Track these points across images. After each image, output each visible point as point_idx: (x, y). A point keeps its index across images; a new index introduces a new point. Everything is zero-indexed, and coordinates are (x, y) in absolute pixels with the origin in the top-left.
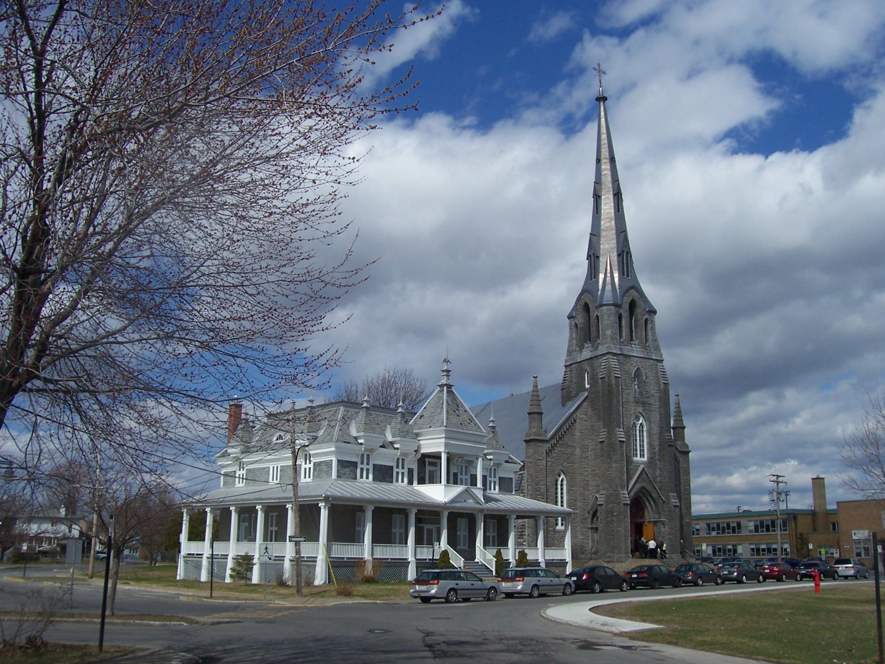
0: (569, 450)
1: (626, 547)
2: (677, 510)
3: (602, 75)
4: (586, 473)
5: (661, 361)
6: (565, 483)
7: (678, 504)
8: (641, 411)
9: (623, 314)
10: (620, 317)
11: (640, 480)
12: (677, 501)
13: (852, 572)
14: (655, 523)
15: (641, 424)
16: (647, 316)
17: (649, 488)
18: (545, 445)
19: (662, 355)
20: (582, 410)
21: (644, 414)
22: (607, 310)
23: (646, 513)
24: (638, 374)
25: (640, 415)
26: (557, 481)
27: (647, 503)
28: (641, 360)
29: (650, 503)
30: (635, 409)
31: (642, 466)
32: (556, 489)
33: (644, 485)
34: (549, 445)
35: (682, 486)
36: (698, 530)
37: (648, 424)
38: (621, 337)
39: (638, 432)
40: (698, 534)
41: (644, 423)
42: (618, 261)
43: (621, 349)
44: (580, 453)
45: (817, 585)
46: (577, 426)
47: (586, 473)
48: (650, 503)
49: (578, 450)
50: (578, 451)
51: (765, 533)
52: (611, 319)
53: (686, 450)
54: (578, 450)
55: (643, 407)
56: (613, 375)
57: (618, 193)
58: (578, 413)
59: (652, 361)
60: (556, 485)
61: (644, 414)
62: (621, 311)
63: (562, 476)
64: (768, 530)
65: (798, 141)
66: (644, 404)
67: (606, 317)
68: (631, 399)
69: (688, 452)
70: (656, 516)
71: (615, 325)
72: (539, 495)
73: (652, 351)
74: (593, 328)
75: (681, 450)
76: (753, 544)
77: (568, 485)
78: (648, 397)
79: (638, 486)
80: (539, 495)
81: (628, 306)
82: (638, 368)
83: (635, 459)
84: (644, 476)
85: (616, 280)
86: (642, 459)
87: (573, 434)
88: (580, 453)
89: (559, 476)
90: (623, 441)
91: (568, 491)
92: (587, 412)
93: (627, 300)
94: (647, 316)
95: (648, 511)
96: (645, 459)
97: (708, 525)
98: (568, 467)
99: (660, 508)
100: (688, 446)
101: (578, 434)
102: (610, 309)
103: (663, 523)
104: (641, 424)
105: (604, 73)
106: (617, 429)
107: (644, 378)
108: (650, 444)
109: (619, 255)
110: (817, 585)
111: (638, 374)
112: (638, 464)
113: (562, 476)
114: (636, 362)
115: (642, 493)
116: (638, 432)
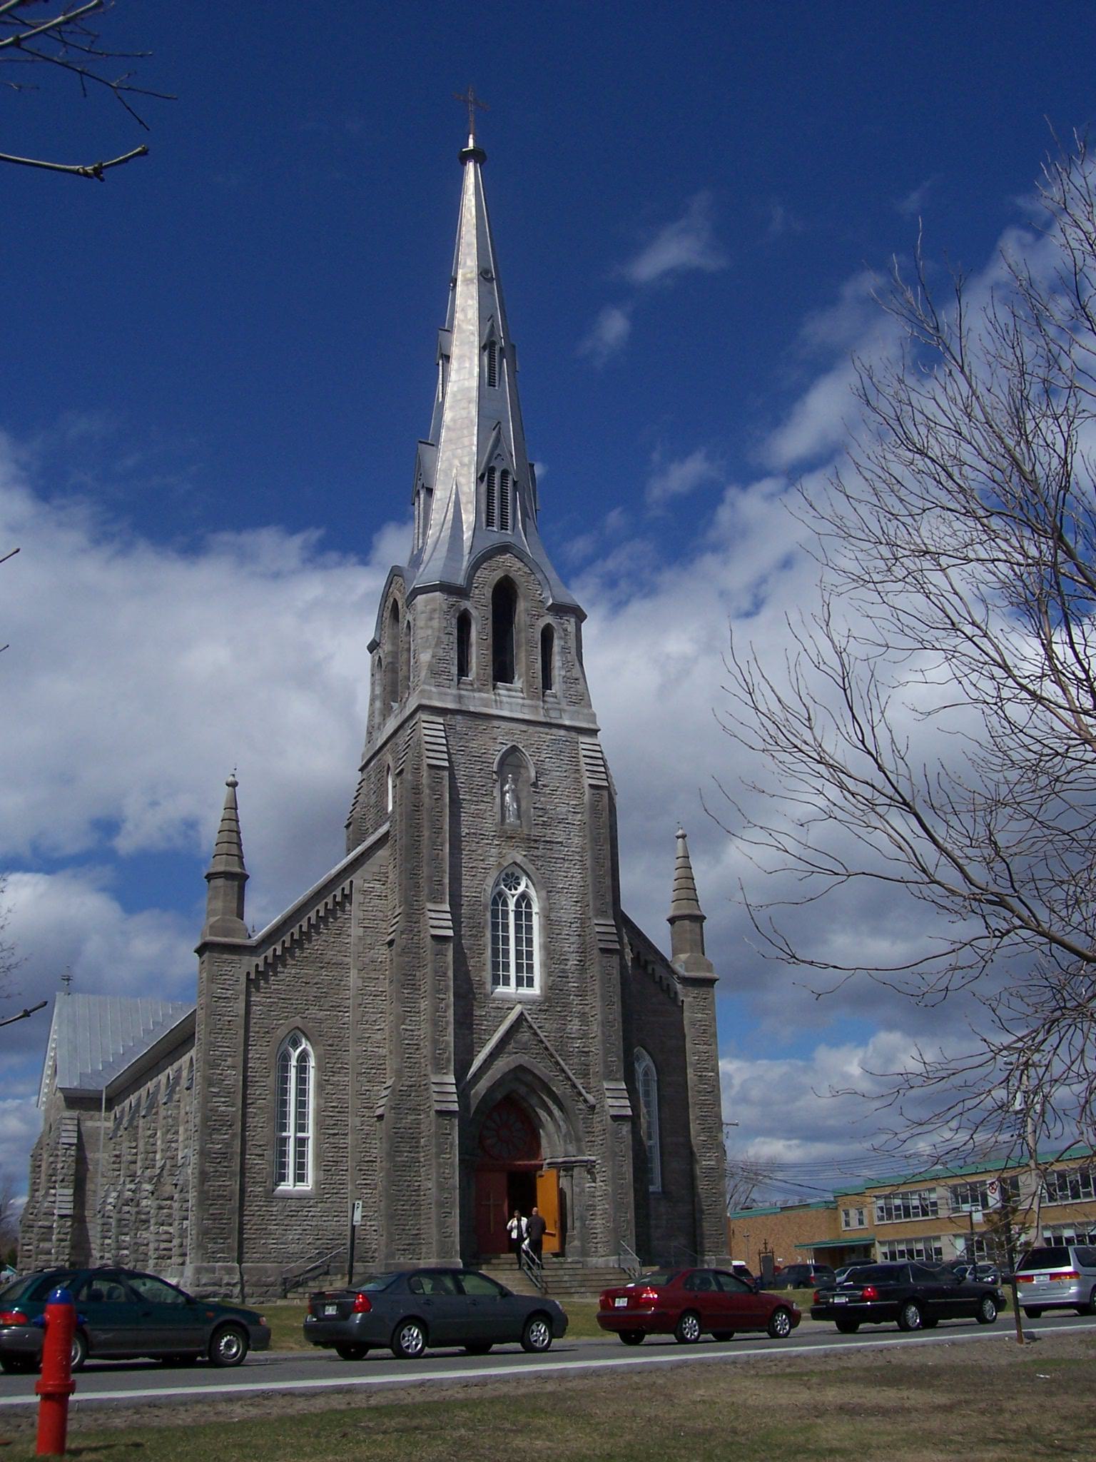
1: (445, 1236)
2: (626, 1129)
4: (378, 1036)
5: (593, 732)
6: (312, 1062)
7: (629, 1112)
8: (519, 859)
9: (474, 612)
10: (464, 622)
11: (511, 1047)
12: (627, 1103)
13: (1074, 1289)
14: (568, 1167)
16: (549, 619)
17: (542, 1068)
18: (246, 959)
19: (594, 715)
20: (370, 867)
21: (530, 868)
22: (427, 603)
23: (544, 1142)
24: (511, 761)
25: (518, 872)
26: (286, 1058)
27: (543, 1114)
28: (524, 727)
29: (550, 1113)
30: (501, 855)
31: (519, 1008)
32: (285, 1080)
33: (524, 1059)
34: (260, 960)
35: (690, 1071)
36: (934, 1204)
37: (544, 893)
38: (463, 670)
40: (935, 1212)
41: (532, 893)
43: (460, 697)
45: (57, 1398)
46: (354, 909)
47: (378, 1036)
48: (550, 1113)
49: (353, 973)
50: (353, 979)
51: (1070, 1201)
52: (435, 623)
54: (353, 973)
58: (357, 879)
59: (562, 732)
60: (285, 1068)
61: (530, 868)
62: (466, 604)
63: (305, 1044)
64: (1076, 1195)
66: (531, 842)
67: (421, 623)
68: (489, 826)
70: (572, 1149)
71: (445, 638)
72: (216, 1095)
73: (564, 706)
75: (687, 974)
76: (1046, 1228)
77: (319, 1068)
79: (503, 1064)
80: (216, 1095)
81: (488, 592)
82: (514, 749)
83: (501, 989)
84: (525, 1036)
85: (467, 535)
86: (525, 991)
89: (295, 1044)
91: (320, 1087)
92: (386, 875)
93: (489, 577)
94: (549, 619)
95: (548, 1135)
96: (536, 991)
97: (954, 1190)
98: (321, 1022)
99: (581, 1126)
101: (355, 931)
102: (433, 599)
103: (589, 1167)
104: (524, 897)
106: (430, 906)
108: (548, 950)
109: (480, 479)
110: (57, 1398)
111: (511, 761)
112: (505, 1005)
113: (305, 1044)
116: (512, 916)
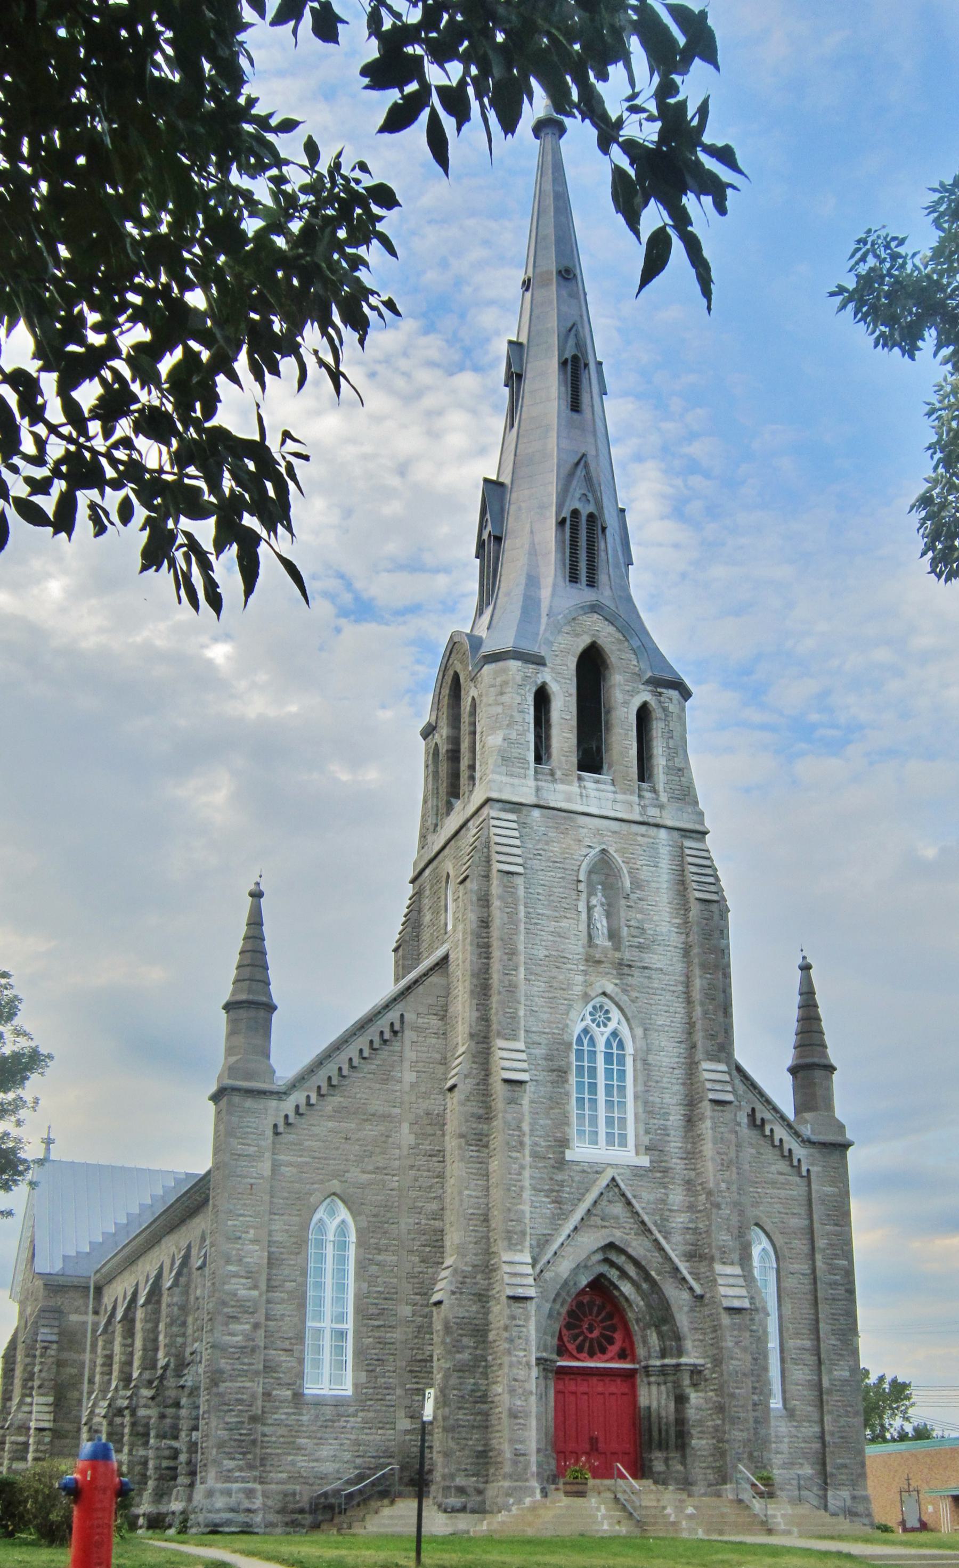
0: (371, 1131)
3: (245, 45)
8: (610, 988)
15: (615, 1034)
19: (701, 814)
21: (624, 999)
25: (609, 1005)
28: (615, 825)
39: (600, 1058)
42: (560, 542)
44: (411, 1139)
53: (837, 1139)
55: (621, 975)
56: (496, 866)
57: (575, 358)
62: (546, 676)
65: (149, 49)
66: (623, 968)
69: (846, 1146)
74: (465, 746)
78: (640, 947)
87: (386, 1078)
88: (411, 1139)
90: (521, 1083)
98: (363, 1187)
100: (842, 1127)
101: (409, 1077)
105: (245, 43)
107: (628, 884)
114: (598, 832)
115: (612, 1264)
116: (600, 1058)
